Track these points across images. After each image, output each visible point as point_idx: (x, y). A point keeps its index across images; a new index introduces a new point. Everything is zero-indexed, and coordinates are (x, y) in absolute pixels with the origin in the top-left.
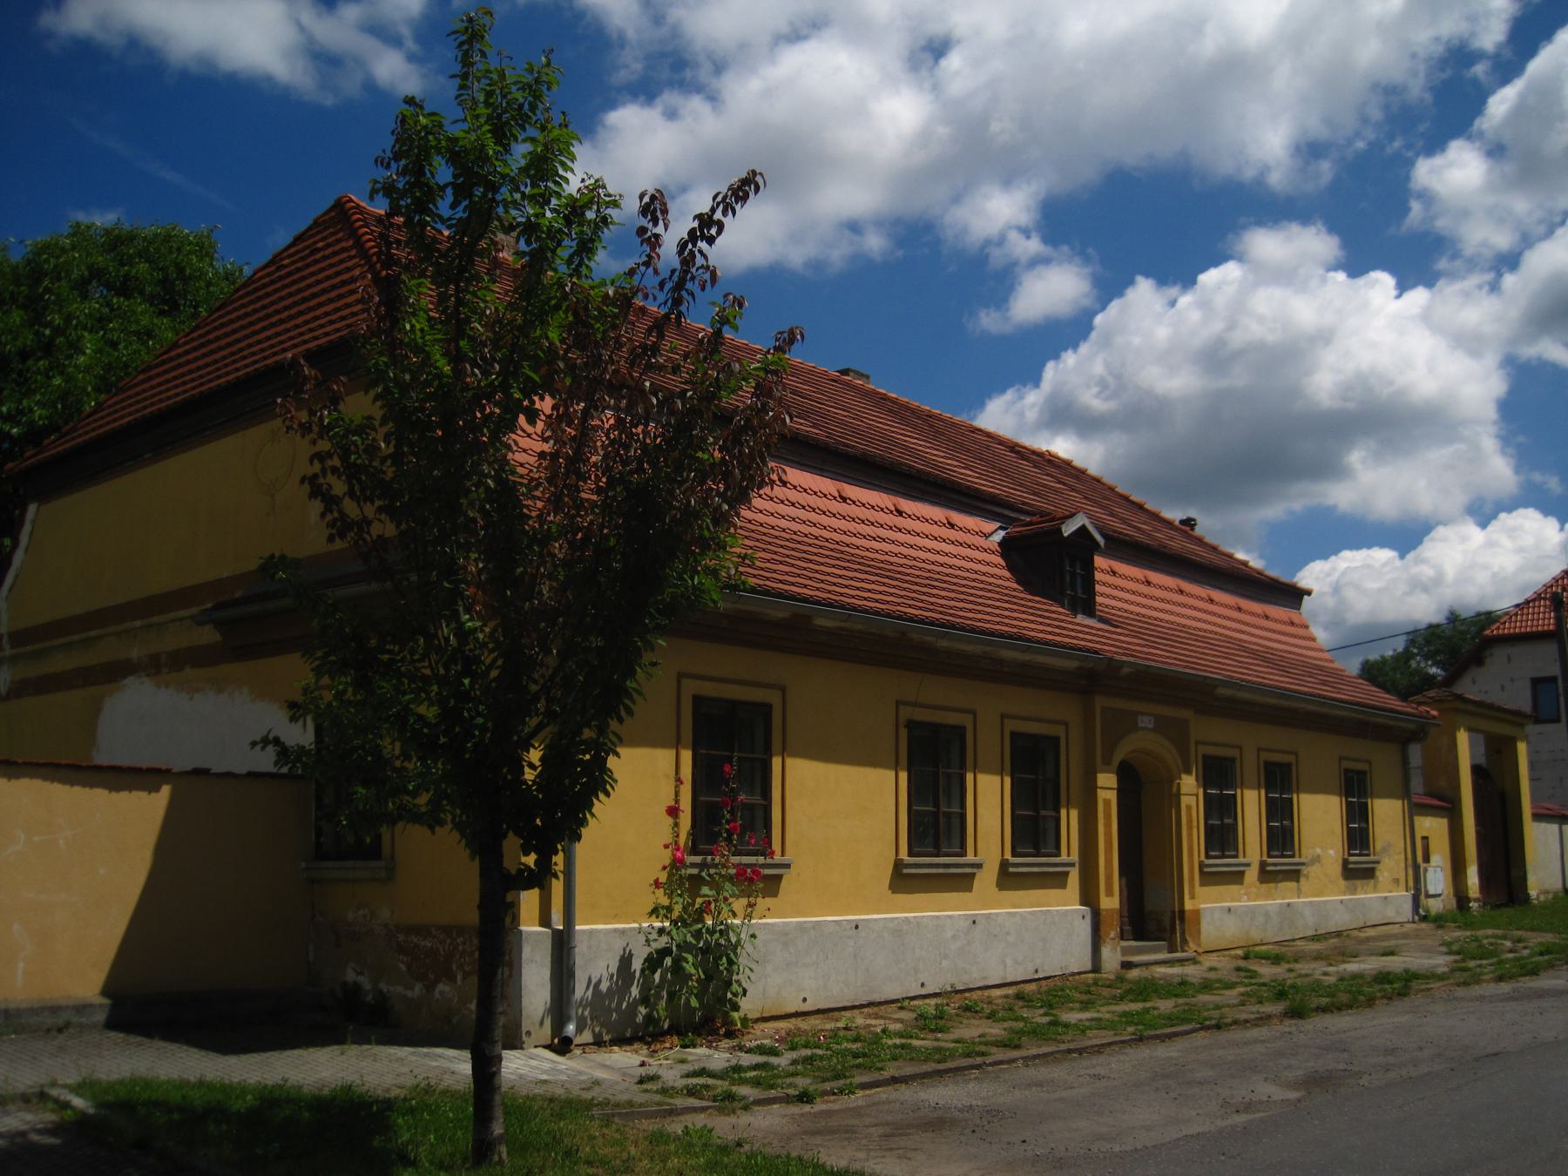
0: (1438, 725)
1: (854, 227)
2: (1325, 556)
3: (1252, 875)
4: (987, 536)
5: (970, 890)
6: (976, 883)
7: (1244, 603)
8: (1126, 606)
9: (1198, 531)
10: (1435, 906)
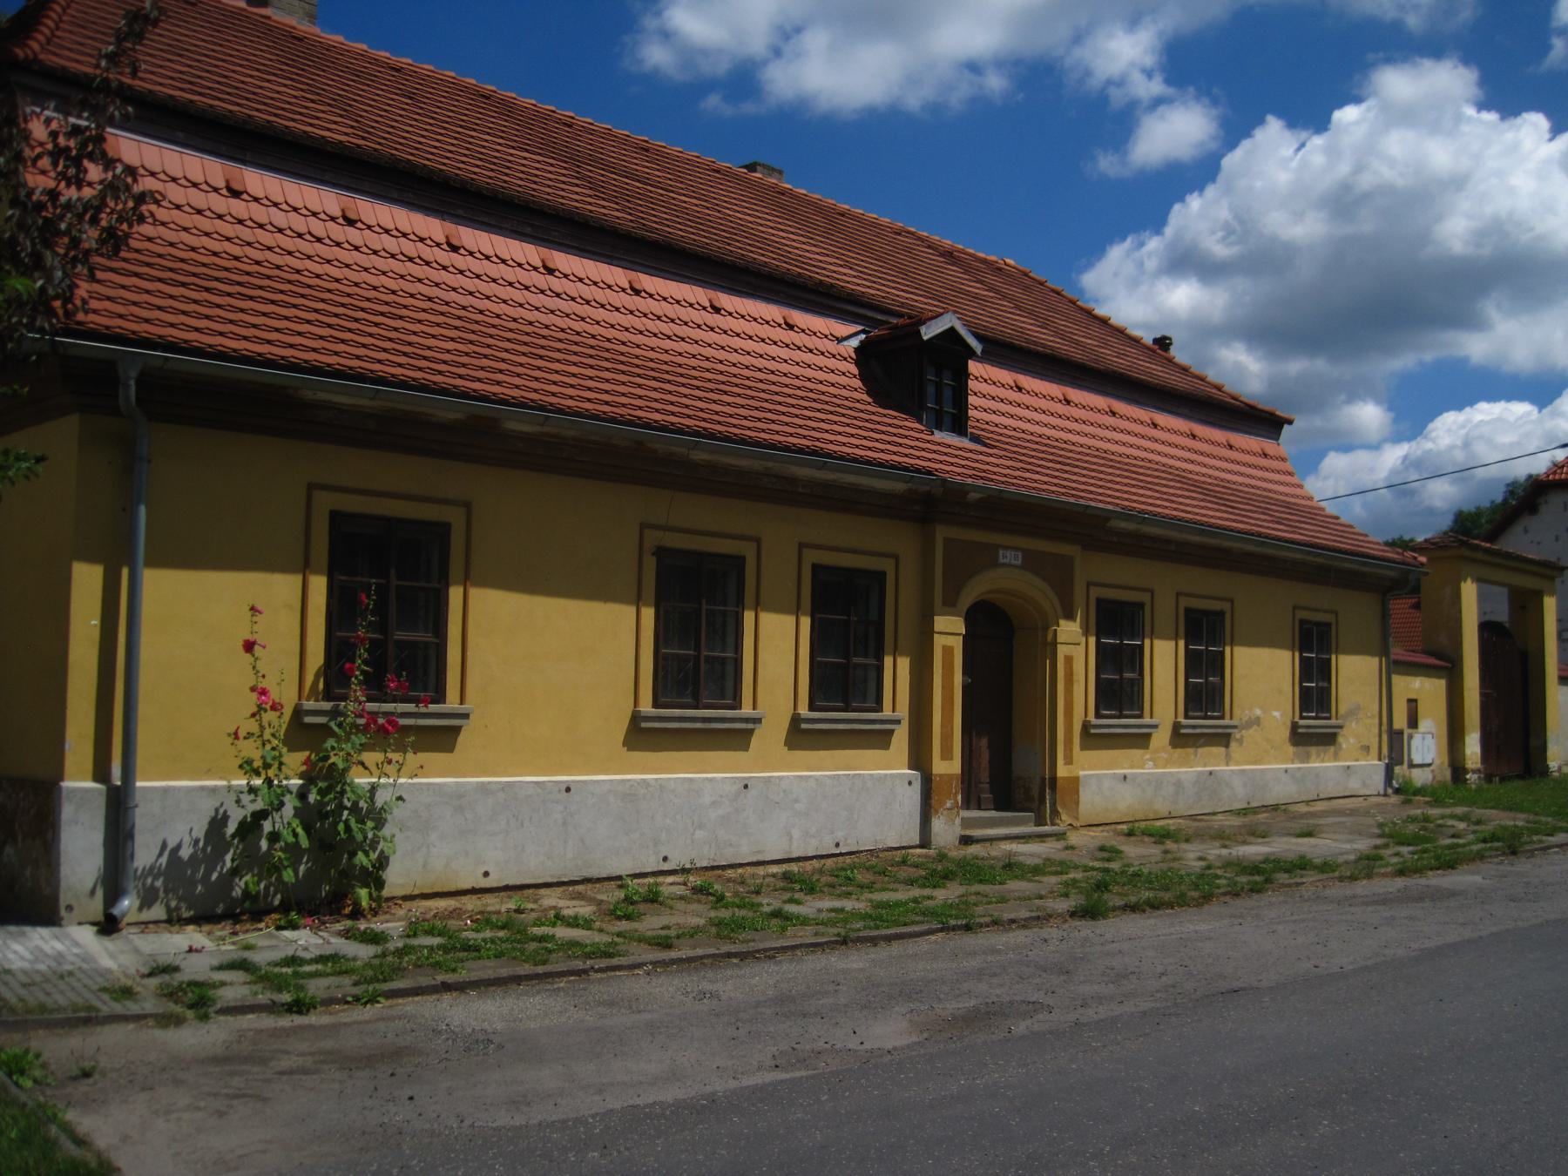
0: (1427, 574)
1: (973, 67)
2: (1459, 407)
3: (1161, 737)
4: (840, 340)
5: (746, 748)
6: (755, 741)
7: (1200, 430)
8: (1021, 424)
9: (1173, 351)
10: (1420, 778)
